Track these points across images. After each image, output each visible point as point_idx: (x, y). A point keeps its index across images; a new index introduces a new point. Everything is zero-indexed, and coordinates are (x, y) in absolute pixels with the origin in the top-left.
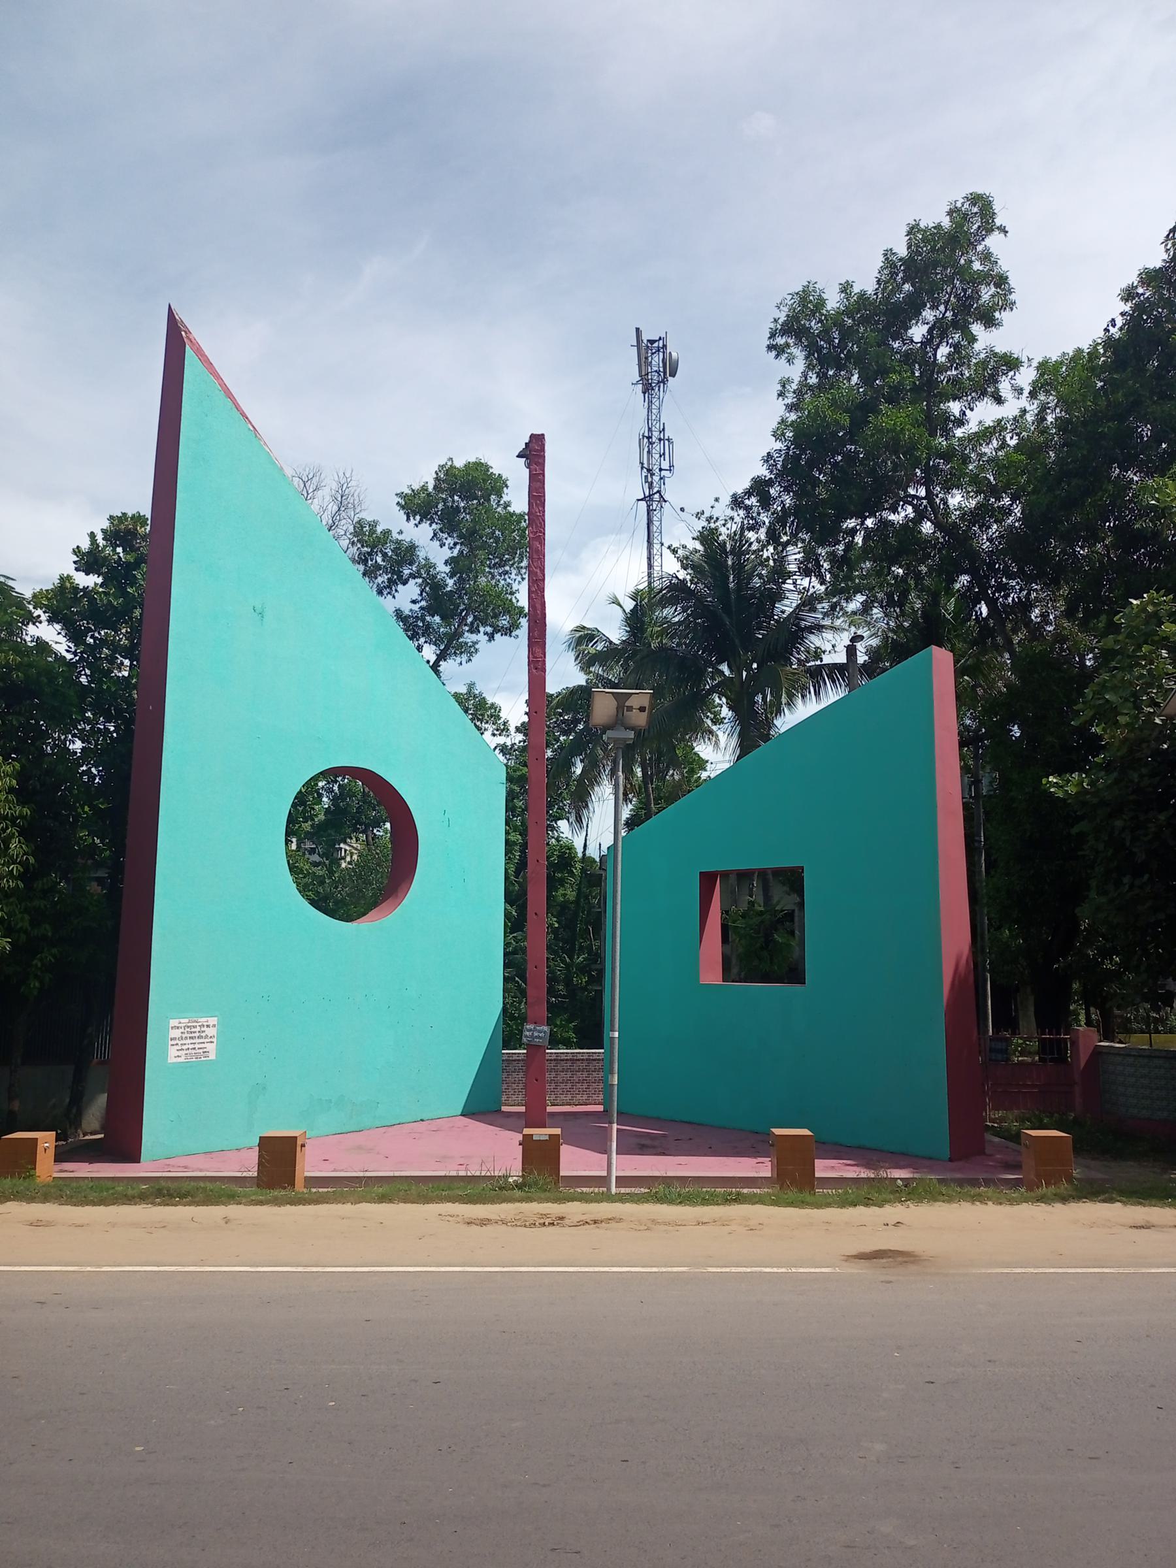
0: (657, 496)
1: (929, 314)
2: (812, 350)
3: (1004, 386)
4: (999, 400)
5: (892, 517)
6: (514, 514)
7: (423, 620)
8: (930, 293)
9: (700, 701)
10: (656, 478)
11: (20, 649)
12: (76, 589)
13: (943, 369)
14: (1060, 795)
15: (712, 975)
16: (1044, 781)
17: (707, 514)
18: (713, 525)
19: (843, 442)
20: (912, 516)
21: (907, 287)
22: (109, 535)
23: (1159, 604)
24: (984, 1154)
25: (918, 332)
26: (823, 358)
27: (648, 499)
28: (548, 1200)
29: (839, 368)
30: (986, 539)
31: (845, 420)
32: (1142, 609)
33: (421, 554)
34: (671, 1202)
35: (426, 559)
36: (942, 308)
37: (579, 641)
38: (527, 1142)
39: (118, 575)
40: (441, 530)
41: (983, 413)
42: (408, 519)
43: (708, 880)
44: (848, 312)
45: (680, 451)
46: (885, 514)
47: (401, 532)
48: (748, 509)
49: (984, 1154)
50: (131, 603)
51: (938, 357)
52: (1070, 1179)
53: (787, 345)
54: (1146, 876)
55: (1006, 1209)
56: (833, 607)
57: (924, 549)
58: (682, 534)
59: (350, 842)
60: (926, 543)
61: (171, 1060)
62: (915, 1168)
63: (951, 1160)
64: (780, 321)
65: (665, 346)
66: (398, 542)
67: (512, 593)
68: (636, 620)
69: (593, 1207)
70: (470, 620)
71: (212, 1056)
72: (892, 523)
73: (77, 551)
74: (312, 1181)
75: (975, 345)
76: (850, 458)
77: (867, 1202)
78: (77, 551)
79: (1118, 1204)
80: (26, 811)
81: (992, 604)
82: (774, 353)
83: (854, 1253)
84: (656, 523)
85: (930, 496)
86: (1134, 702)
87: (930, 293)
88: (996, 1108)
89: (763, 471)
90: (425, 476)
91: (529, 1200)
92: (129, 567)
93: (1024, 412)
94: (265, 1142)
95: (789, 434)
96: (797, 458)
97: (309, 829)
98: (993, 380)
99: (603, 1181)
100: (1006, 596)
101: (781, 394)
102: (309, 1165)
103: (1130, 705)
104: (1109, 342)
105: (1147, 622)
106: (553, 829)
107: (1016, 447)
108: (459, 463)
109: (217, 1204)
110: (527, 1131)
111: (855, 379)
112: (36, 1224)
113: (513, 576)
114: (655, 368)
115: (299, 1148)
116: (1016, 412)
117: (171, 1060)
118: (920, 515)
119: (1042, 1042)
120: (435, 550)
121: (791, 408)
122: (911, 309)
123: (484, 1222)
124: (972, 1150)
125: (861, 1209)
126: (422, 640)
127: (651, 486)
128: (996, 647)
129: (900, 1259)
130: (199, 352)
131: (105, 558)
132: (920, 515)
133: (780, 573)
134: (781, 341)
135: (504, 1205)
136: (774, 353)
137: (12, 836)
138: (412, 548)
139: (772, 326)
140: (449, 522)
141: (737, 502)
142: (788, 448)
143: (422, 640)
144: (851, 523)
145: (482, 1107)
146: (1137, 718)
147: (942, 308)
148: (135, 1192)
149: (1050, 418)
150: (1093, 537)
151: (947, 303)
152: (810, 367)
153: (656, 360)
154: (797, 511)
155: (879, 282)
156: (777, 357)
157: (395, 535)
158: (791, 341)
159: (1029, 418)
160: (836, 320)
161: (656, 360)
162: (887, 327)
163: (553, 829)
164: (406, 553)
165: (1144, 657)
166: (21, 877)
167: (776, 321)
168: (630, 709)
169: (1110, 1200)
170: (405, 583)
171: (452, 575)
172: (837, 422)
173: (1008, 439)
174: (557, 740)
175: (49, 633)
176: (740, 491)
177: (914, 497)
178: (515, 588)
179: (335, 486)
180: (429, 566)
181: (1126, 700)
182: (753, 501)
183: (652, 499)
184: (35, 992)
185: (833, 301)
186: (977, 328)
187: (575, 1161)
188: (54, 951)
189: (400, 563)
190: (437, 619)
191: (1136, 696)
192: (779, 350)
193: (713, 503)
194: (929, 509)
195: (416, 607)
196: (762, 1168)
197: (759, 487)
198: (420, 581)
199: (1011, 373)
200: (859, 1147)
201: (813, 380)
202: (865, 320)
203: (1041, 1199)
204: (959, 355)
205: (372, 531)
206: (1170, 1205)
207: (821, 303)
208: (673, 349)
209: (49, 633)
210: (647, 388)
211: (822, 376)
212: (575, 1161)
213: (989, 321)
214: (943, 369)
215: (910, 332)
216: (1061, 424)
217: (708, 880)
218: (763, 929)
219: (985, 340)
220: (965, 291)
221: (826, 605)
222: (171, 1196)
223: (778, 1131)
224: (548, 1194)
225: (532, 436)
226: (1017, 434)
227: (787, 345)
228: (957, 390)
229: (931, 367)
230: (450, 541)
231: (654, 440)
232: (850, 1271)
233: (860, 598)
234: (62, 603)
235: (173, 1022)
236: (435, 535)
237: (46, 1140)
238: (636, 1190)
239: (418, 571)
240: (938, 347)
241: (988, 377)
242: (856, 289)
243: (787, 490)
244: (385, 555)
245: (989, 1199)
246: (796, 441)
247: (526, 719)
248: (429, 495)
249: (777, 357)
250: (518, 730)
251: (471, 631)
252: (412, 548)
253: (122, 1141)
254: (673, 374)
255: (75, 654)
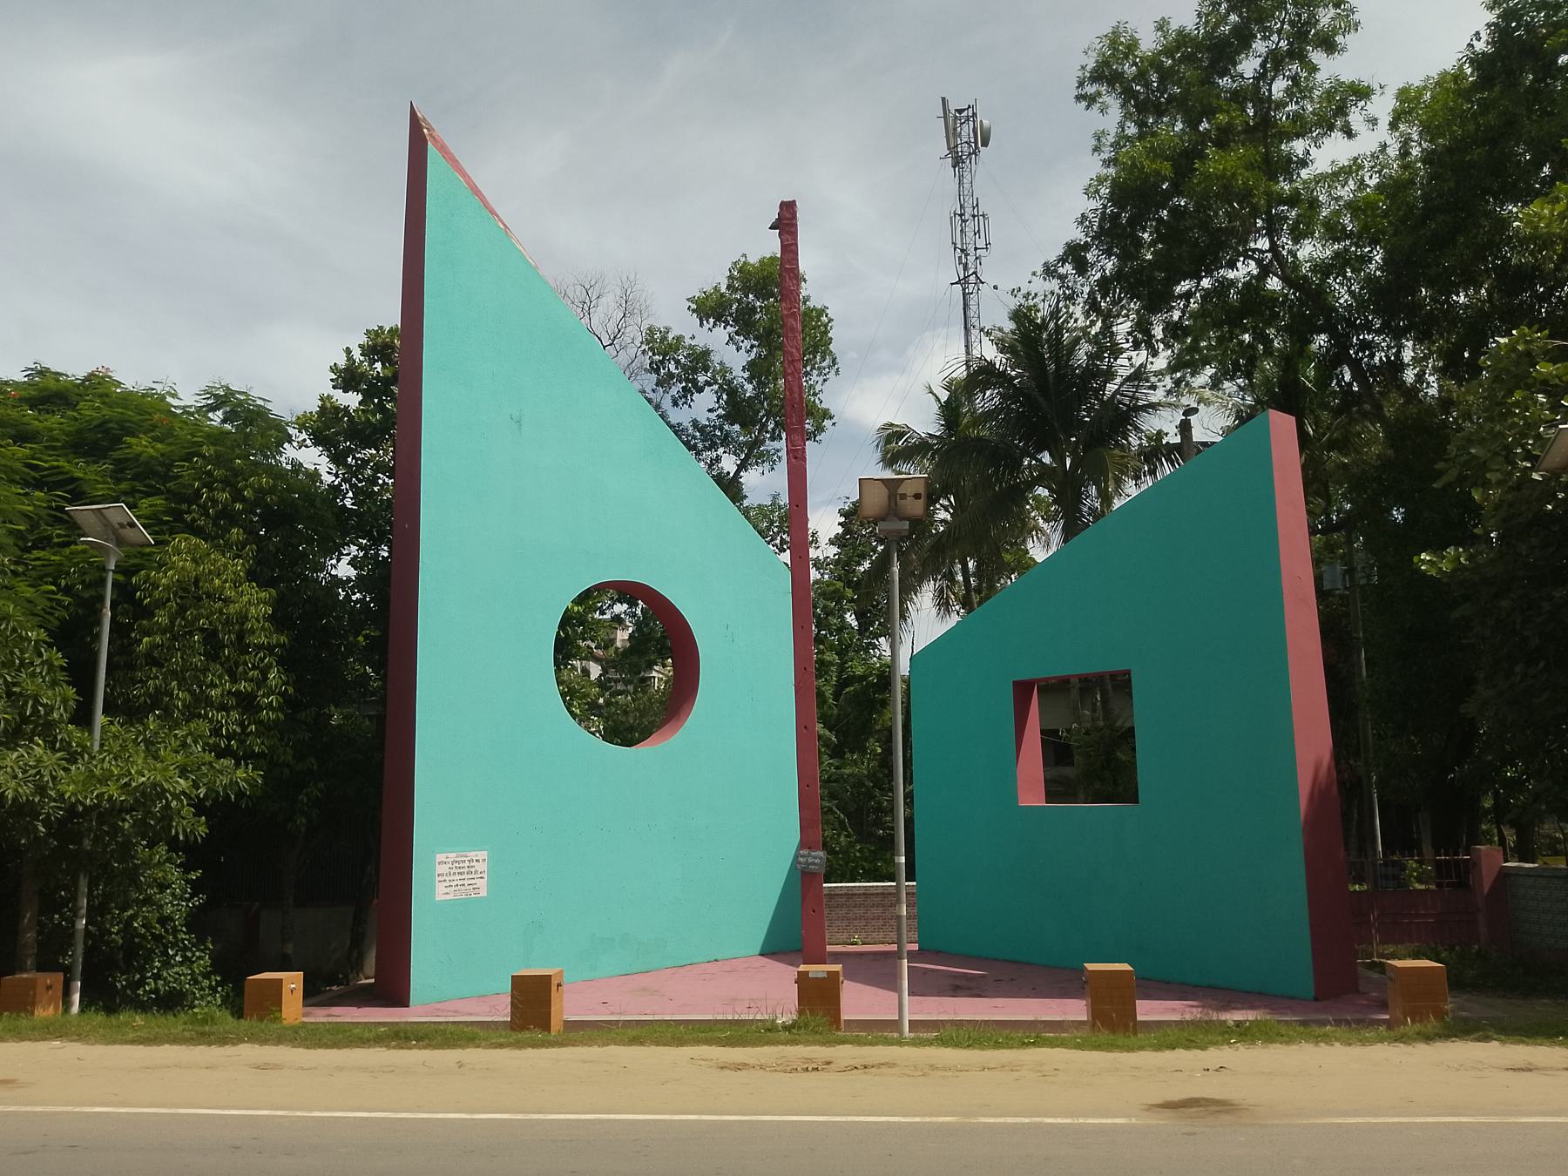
0: (972, 278)
1: (1260, 46)
2: (1128, 95)
3: (1355, 118)
4: (1349, 133)
5: (1231, 275)
6: (814, 309)
7: (721, 429)
8: (1260, 21)
9: (1018, 494)
10: (971, 259)
11: (277, 473)
12: (337, 409)
13: (1281, 105)
14: (1433, 573)
15: (1032, 797)
16: (1415, 559)
17: (1024, 291)
18: (1031, 303)
19: (1168, 195)
20: (1255, 272)
21: (1233, 18)
22: (367, 351)
23: (1531, 342)
24: (1358, 991)
25: (1248, 66)
26: (1142, 107)
27: (962, 282)
28: (815, 1043)
29: (1160, 113)
30: (1342, 294)
31: (1166, 168)
32: (1511, 348)
33: (716, 358)
34: (957, 1045)
35: (721, 363)
36: (1275, 37)
37: (888, 440)
38: (802, 979)
39: (373, 390)
40: (737, 333)
41: (1329, 153)
42: (701, 325)
43: (1023, 690)
44: (1168, 51)
45: (996, 230)
46: (1222, 272)
47: (693, 337)
48: (1062, 278)
49: (1358, 991)
50: (389, 419)
51: (1274, 91)
52: (1440, 1015)
53: (1099, 94)
54: (1542, 664)
55: (1357, 1051)
56: (1177, 383)
57: (1272, 309)
58: (997, 315)
59: (630, 664)
60: (1272, 298)
61: (439, 897)
62: (1273, 1009)
63: (1316, 999)
64: (1089, 68)
65: (974, 115)
66: (691, 347)
67: (815, 394)
68: (950, 412)
69: (867, 1050)
70: (771, 426)
71: (483, 893)
72: (1232, 283)
73: (334, 368)
74: (571, 1026)
75: (1318, 76)
76: (1175, 211)
77: (1189, 1044)
78: (334, 368)
79: (1495, 1043)
80: (283, 639)
81: (1355, 365)
82: (1084, 104)
83: (1159, 1101)
84: (973, 308)
85: (1274, 248)
86: (1506, 458)
87: (1260, 21)
88: (1383, 942)
89: (1079, 235)
90: (715, 276)
91: (794, 1042)
92: (388, 381)
93: (1384, 147)
94: (517, 981)
95: (1104, 191)
96: (1115, 217)
97: (352, 573)
98: (1342, 111)
99: (895, 1025)
100: (1372, 356)
101: (1096, 149)
102: (568, 1007)
103: (1501, 459)
104: (1478, 61)
105: (1517, 364)
106: (875, 647)
107: (1378, 187)
108: (753, 259)
109: (454, 1046)
110: (803, 968)
111: (1179, 126)
112: (264, 1067)
113: (814, 378)
114: (965, 138)
115: (554, 988)
116: (1375, 147)
117: (439, 897)
118: (1265, 271)
119: (1438, 864)
120: (732, 354)
121: (1107, 163)
122: (1243, 39)
123: (739, 1067)
124: (1336, 988)
125: (1180, 1052)
126: (721, 450)
127: (966, 268)
128: (1365, 415)
129: (1213, 1108)
130: (443, 149)
131: (363, 374)
132: (1265, 271)
133: (1106, 346)
134: (1090, 89)
135: (766, 1049)
136: (1084, 104)
137: (270, 666)
138: (706, 353)
139: (1080, 74)
140: (745, 323)
141: (1049, 271)
142: (1105, 207)
143: (721, 450)
144: (1184, 286)
145: (776, 948)
146: (1511, 474)
147: (1275, 37)
148: (371, 1035)
149: (1415, 152)
150: (1470, 280)
151: (1279, 32)
152: (1127, 116)
153: (966, 131)
154: (1118, 275)
155: (1199, 16)
156: (1087, 108)
157: (688, 341)
158: (1103, 89)
159: (1393, 151)
160: (1154, 62)
161: (966, 131)
162: (1213, 64)
163: (875, 647)
164: (701, 359)
165: (1517, 404)
166: (280, 708)
167: (1083, 68)
168: (903, 496)
169: (1486, 1039)
170: (700, 390)
171: (749, 380)
172: (1158, 173)
173: (1367, 179)
174: (874, 550)
175: (313, 458)
176: (1052, 258)
177: (1254, 251)
178: (818, 388)
179: (619, 292)
180: (724, 370)
181: (1496, 454)
182: (1068, 269)
183: (967, 281)
184: (303, 829)
185: (1149, 42)
186: (1317, 56)
187: (858, 1001)
188: (321, 785)
189: (695, 371)
190: (737, 427)
191: (1508, 449)
192: (1091, 100)
193: (1030, 277)
194: (1278, 263)
195: (713, 416)
196: (1076, 1010)
197: (1074, 253)
198: (716, 387)
199: (1361, 104)
200: (1209, 987)
201: (1132, 130)
202: (1187, 59)
203: (1403, 1039)
204: (1298, 89)
205: (664, 338)
206: (1561, 1044)
207: (1133, 45)
208: (984, 119)
209: (313, 458)
210: (957, 162)
211: (1141, 124)
212: (858, 1001)
213: (1328, 44)
214: (1281, 105)
215: (1239, 68)
216: (1428, 158)
217: (1023, 690)
218: (1091, 744)
219: (1329, 69)
220: (1299, 16)
221: (1168, 382)
222: (408, 1039)
223: (1090, 967)
224: (818, 1037)
225: (783, 204)
226: (1380, 172)
227: (1099, 94)
228: (1300, 127)
229: (1265, 105)
230: (747, 344)
231: (968, 216)
232: (1154, 1122)
233: (1210, 371)
234: (327, 427)
235: (440, 857)
236: (731, 338)
237: (292, 981)
238: (926, 1036)
239: (713, 377)
240: (1273, 79)
241: (1338, 107)
242: (1174, 26)
243: (1108, 253)
244: (678, 362)
245: (1337, 1040)
246: (1112, 198)
247: (840, 530)
248: (722, 295)
249: (1087, 108)
250: (832, 542)
251: (773, 439)
252: (706, 353)
253: (393, 990)
254: (985, 144)
255: (337, 476)
